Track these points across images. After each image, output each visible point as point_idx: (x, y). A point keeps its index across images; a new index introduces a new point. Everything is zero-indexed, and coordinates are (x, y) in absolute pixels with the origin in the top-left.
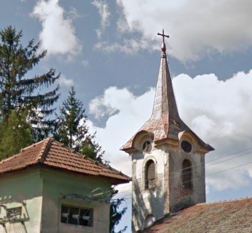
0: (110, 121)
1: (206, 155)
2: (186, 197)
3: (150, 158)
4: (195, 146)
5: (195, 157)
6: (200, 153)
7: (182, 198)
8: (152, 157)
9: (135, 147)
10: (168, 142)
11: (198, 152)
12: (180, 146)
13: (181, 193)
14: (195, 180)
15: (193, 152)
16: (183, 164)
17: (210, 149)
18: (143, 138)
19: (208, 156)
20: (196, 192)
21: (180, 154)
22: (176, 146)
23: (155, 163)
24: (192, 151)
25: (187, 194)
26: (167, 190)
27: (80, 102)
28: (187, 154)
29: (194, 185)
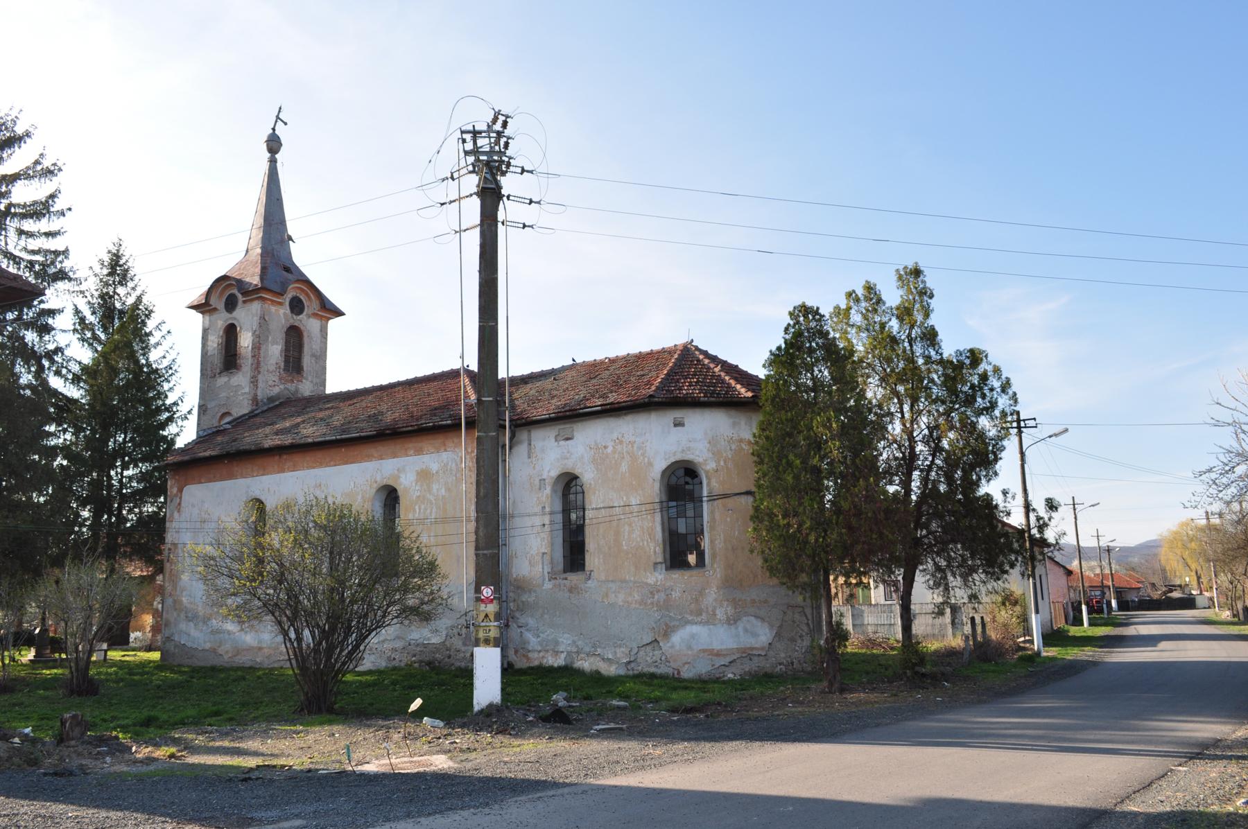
0: (152, 315)
1: (331, 322)
2: (289, 386)
3: (231, 322)
4: (311, 305)
5: (310, 325)
6: (321, 317)
7: (282, 387)
8: (235, 319)
9: (211, 303)
10: (264, 295)
11: (315, 315)
12: (287, 303)
13: (280, 379)
14: (307, 361)
15: (307, 315)
16: (286, 333)
17: (339, 313)
18: (302, 290)
19: (334, 324)
20: (310, 379)
21: (282, 315)
22: (280, 304)
23: (238, 329)
24: (305, 313)
25: (292, 381)
26: (279, 399)
27: (415, 535)
28: (295, 317)
29: (305, 369)
